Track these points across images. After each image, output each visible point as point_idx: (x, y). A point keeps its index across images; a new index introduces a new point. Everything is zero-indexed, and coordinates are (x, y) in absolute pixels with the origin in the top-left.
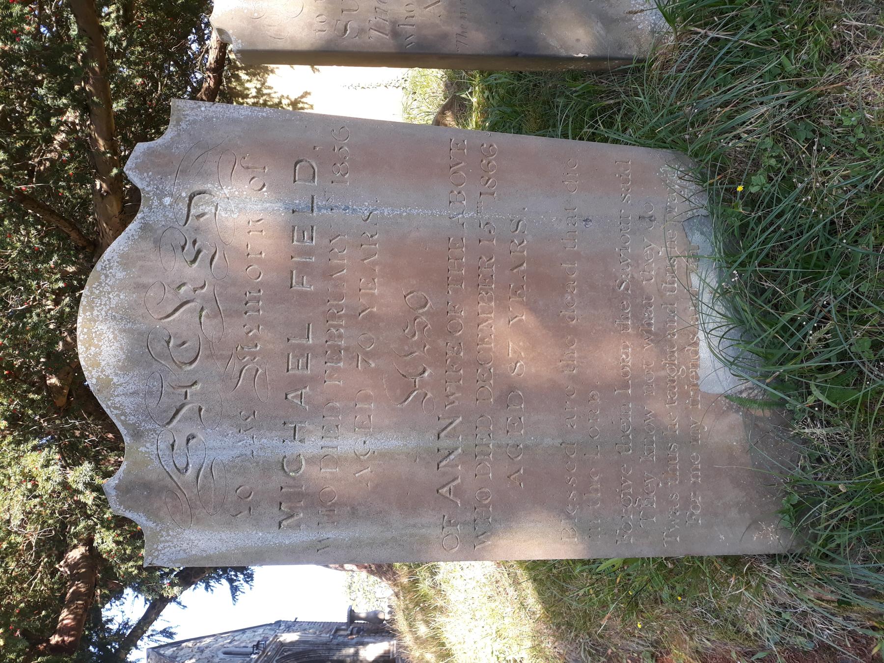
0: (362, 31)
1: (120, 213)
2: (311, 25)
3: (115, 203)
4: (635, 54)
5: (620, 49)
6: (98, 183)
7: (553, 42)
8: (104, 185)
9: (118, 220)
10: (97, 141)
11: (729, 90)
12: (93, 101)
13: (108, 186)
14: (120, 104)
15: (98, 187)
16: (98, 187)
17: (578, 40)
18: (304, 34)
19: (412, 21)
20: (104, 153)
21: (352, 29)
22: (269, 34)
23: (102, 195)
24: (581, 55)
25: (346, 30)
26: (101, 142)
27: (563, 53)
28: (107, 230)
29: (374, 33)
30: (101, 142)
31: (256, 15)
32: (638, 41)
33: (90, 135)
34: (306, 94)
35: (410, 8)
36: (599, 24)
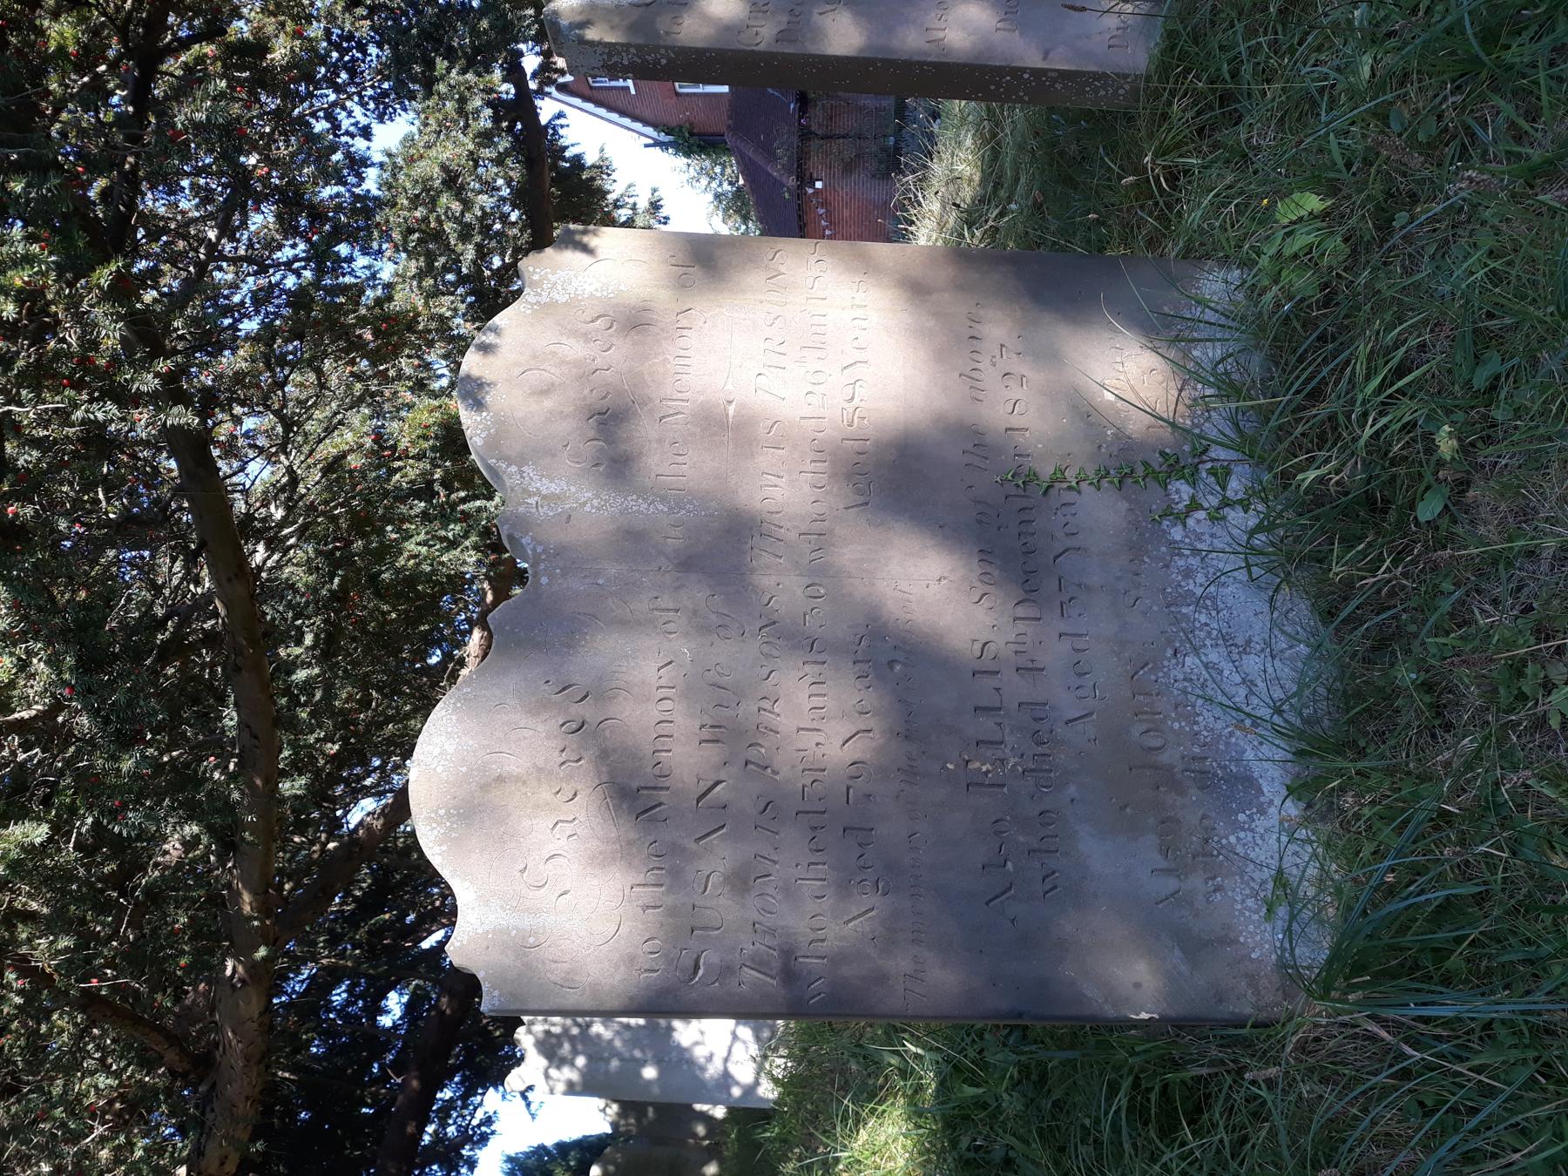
0: (727, 970)
1: (261, 1014)
2: (632, 959)
3: (254, 999)
4: (1248, 1010)
5: (1220, 1001)
6: (230, 964)
7: (1091, 991)
8: (240, 969)
9: (255, 1025)
10: (239, 894)
11: (1433, 992)
12: (243, 839)
13: (246, 971)
14: (297, 785)
15: (229, 972)
16: (229, 972)
17: (1137, 985)
18: (618, 977)
19: (823, 948)
20: (251, 918)
21: (708, 966)
22: (553, 978)
23: (233, 986)
24: (1144, 1016)
25: (696, 967)
26: (246, 897)
27: (1110, 1011)
28: (234, 1043)
29: (750, 974)
30: (246, 897)
31: (531, 940)
32: (1252, 979)
33: (229, 886)
34: (647, 146)
35: (816, 923)
36: (1177, 952)
